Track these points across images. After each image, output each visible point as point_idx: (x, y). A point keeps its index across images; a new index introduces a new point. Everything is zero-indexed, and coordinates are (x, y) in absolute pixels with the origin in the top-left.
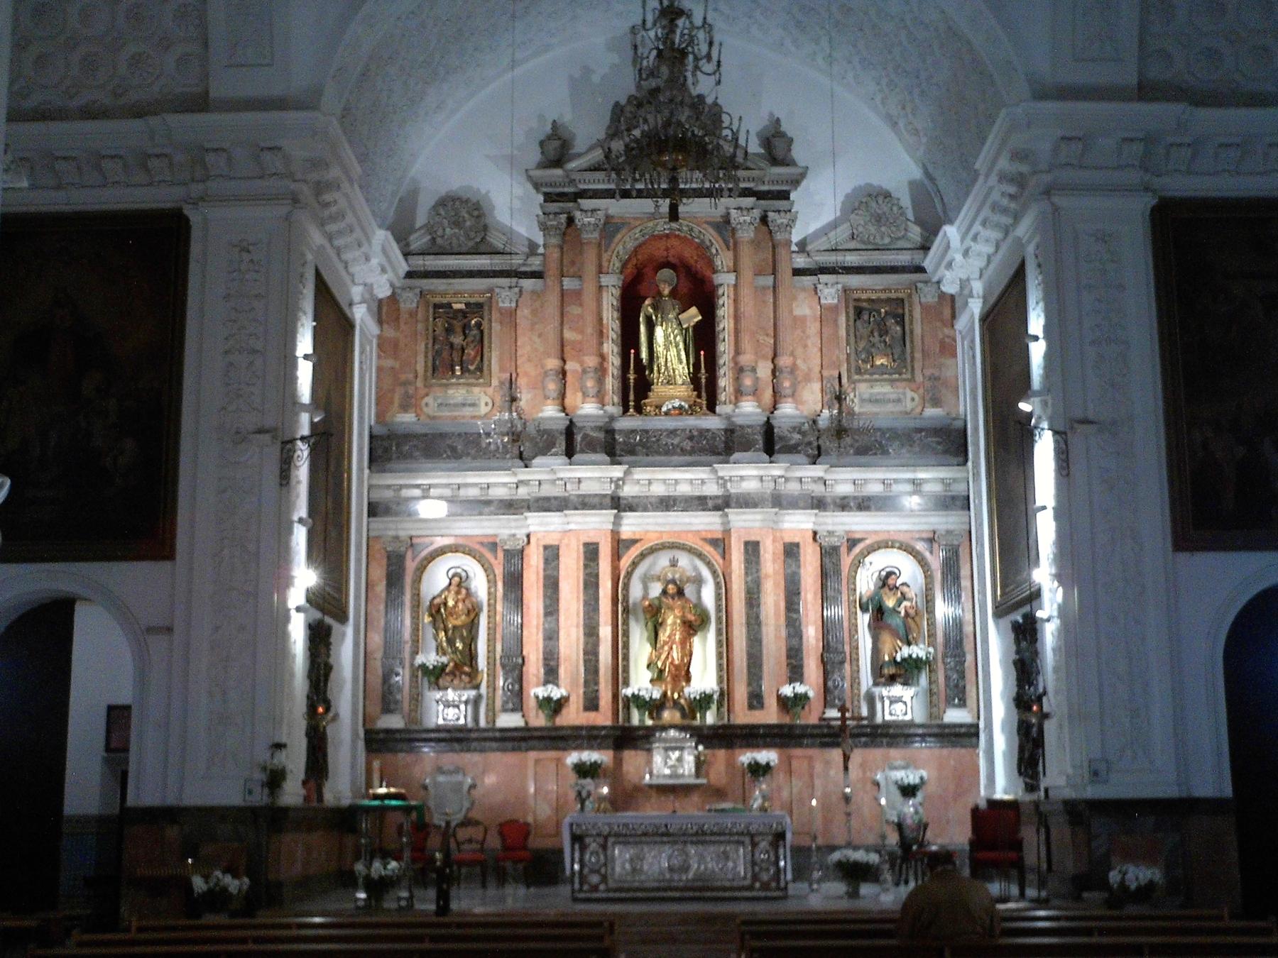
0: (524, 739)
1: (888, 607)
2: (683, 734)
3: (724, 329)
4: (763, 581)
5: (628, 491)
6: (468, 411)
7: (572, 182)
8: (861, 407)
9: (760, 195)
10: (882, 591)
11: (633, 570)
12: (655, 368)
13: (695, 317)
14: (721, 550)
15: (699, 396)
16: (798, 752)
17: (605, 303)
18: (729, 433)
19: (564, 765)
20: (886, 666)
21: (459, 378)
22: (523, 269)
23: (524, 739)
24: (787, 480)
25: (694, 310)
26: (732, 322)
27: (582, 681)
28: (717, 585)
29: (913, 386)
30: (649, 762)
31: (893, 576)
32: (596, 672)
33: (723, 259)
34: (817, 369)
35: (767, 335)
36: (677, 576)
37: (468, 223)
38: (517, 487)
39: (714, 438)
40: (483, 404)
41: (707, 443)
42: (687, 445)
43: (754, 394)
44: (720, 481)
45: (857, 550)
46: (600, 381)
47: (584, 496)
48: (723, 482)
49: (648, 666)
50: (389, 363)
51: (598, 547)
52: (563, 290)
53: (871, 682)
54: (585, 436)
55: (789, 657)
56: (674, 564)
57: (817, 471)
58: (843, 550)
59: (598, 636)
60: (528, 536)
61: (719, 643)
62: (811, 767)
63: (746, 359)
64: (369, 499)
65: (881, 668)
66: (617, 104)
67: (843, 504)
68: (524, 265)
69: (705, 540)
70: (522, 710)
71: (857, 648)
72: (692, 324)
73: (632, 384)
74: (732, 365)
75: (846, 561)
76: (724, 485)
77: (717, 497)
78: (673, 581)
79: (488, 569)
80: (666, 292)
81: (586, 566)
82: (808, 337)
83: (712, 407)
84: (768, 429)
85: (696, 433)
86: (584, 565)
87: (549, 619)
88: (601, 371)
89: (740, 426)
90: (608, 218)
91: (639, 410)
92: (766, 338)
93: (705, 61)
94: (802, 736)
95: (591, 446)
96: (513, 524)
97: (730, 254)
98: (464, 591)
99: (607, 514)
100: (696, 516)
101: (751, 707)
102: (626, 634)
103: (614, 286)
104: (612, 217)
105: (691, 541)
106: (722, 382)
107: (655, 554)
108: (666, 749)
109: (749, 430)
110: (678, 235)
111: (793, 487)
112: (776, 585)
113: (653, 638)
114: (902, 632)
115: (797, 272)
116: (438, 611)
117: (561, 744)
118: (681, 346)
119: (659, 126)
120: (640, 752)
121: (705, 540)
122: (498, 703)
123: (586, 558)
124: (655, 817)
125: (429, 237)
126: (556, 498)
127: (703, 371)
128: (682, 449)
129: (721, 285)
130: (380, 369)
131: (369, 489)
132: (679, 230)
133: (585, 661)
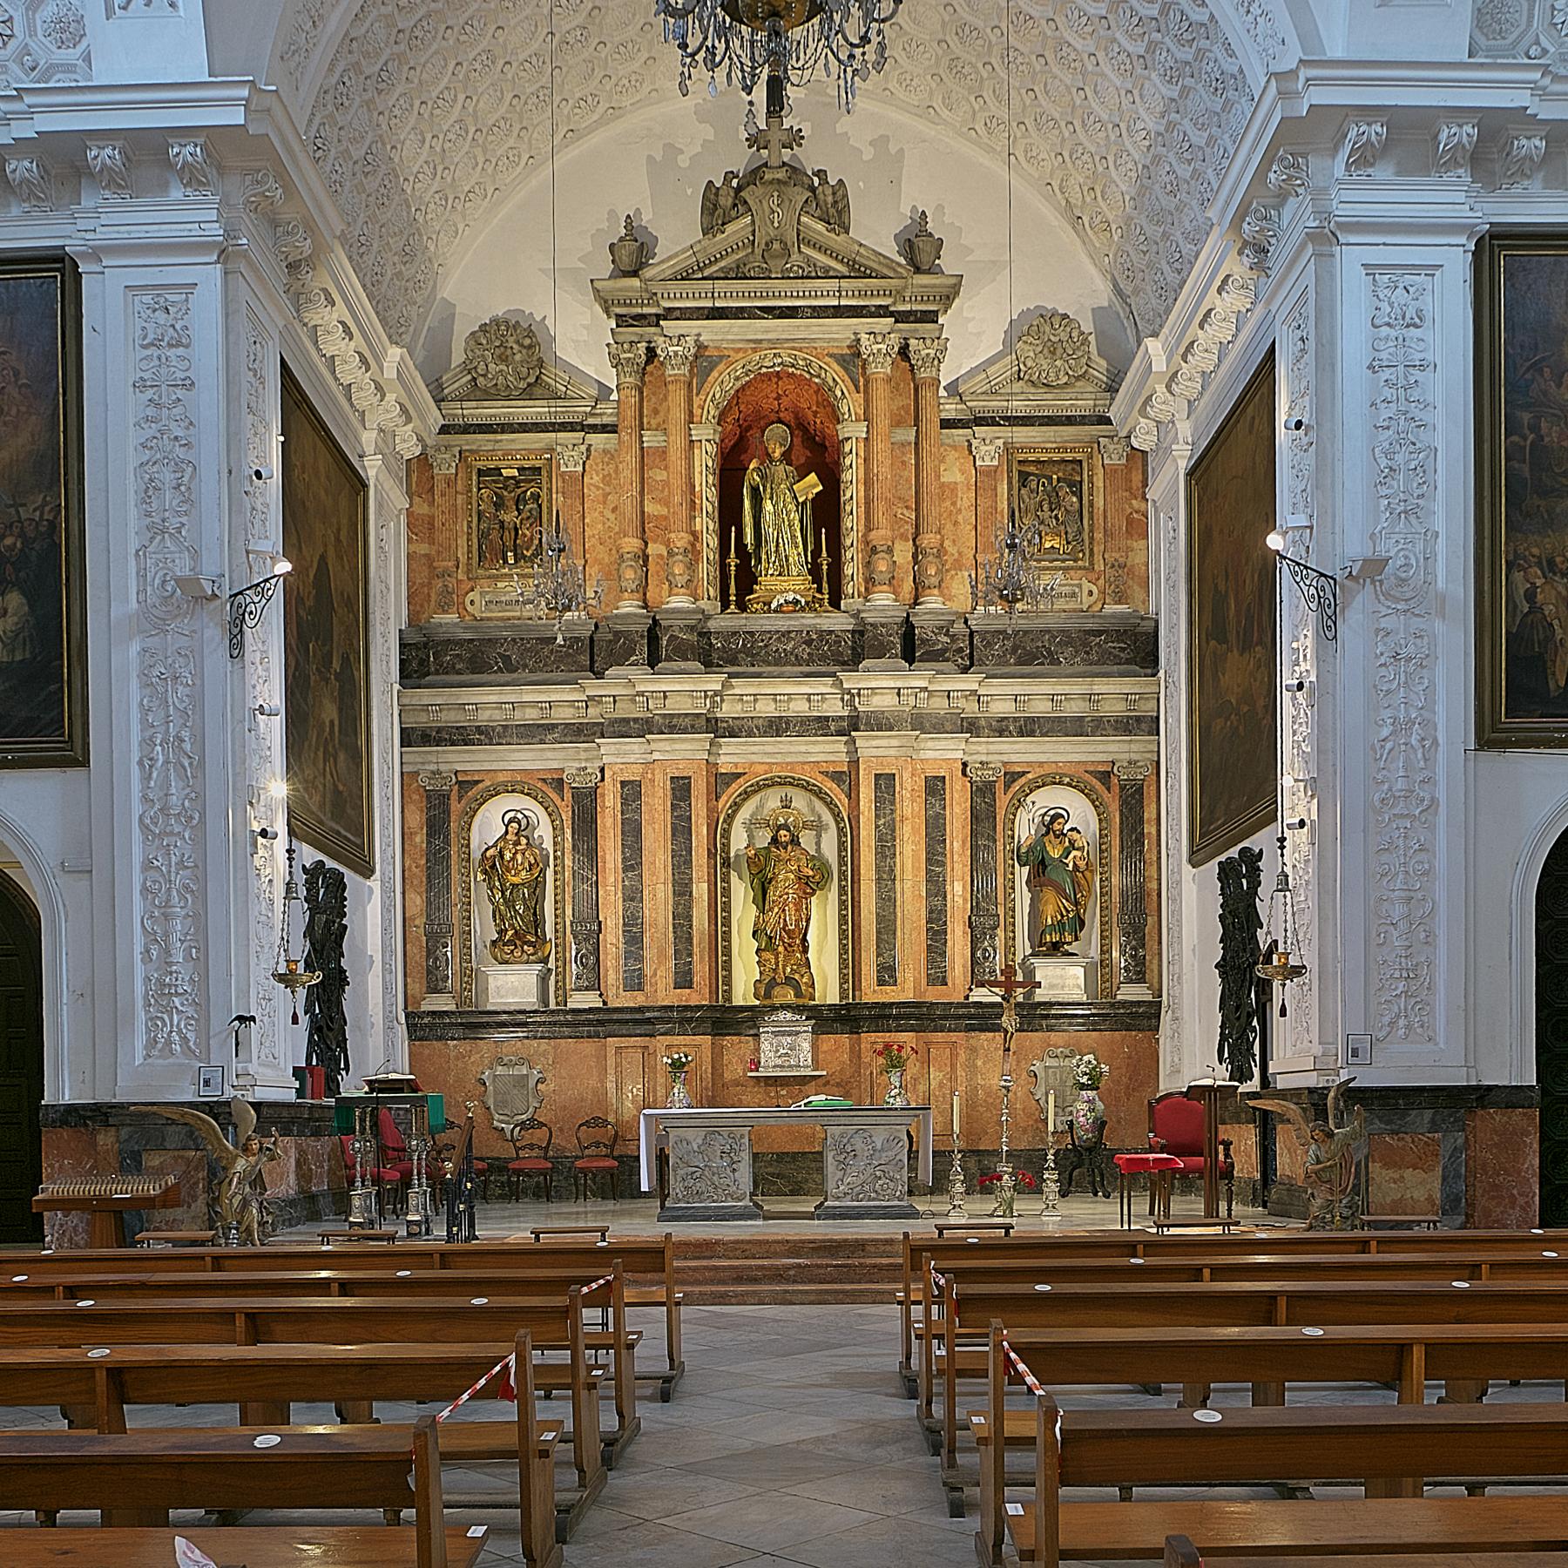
4: (898, 825)
5: (728, 710)
9: (901, 317)
10: (1046, 839)
11: (735, 812)
13: (815, 486)
14: (846, 788)
15: (819, 590)
17: (697, 464)
18: (857, 636)
20: (1047, 930)
22: (591, 421)
26: (862, 488)
28: (841, 831)
29: (1093, 576)
31: (1061, 820)
32: (690, 940)
35: (907, 507)
37: (518, 357)
45: (1016, 786)
46: (692, 566)
50: (423, 548)
57: (970, 682)
58: (1000, 786)
60: (602, 770)
61: (842, 903)
62: (954, 1056)
63: (879, 536)
67: (1001, 728)
69: (826, 774)
75: (1002, 801)
76: (851, 703)
78: (786, 827)
83: (835, 603)
84: (908, 628)
85: (814, 637)
91: (742, 607)
95: (682, 651)
96: (583, 755)
101: (881, 982)
102: (727, 892)
103: (708, 441)
106: (848, 570)
111: (939, 704)
115: (947, 424)
116: (493, 866)
117: (647, 1028)
121: (826, 774)
122: (571, 982)
123: (674, 796)
126: (636, 720)
127: (824, 554)
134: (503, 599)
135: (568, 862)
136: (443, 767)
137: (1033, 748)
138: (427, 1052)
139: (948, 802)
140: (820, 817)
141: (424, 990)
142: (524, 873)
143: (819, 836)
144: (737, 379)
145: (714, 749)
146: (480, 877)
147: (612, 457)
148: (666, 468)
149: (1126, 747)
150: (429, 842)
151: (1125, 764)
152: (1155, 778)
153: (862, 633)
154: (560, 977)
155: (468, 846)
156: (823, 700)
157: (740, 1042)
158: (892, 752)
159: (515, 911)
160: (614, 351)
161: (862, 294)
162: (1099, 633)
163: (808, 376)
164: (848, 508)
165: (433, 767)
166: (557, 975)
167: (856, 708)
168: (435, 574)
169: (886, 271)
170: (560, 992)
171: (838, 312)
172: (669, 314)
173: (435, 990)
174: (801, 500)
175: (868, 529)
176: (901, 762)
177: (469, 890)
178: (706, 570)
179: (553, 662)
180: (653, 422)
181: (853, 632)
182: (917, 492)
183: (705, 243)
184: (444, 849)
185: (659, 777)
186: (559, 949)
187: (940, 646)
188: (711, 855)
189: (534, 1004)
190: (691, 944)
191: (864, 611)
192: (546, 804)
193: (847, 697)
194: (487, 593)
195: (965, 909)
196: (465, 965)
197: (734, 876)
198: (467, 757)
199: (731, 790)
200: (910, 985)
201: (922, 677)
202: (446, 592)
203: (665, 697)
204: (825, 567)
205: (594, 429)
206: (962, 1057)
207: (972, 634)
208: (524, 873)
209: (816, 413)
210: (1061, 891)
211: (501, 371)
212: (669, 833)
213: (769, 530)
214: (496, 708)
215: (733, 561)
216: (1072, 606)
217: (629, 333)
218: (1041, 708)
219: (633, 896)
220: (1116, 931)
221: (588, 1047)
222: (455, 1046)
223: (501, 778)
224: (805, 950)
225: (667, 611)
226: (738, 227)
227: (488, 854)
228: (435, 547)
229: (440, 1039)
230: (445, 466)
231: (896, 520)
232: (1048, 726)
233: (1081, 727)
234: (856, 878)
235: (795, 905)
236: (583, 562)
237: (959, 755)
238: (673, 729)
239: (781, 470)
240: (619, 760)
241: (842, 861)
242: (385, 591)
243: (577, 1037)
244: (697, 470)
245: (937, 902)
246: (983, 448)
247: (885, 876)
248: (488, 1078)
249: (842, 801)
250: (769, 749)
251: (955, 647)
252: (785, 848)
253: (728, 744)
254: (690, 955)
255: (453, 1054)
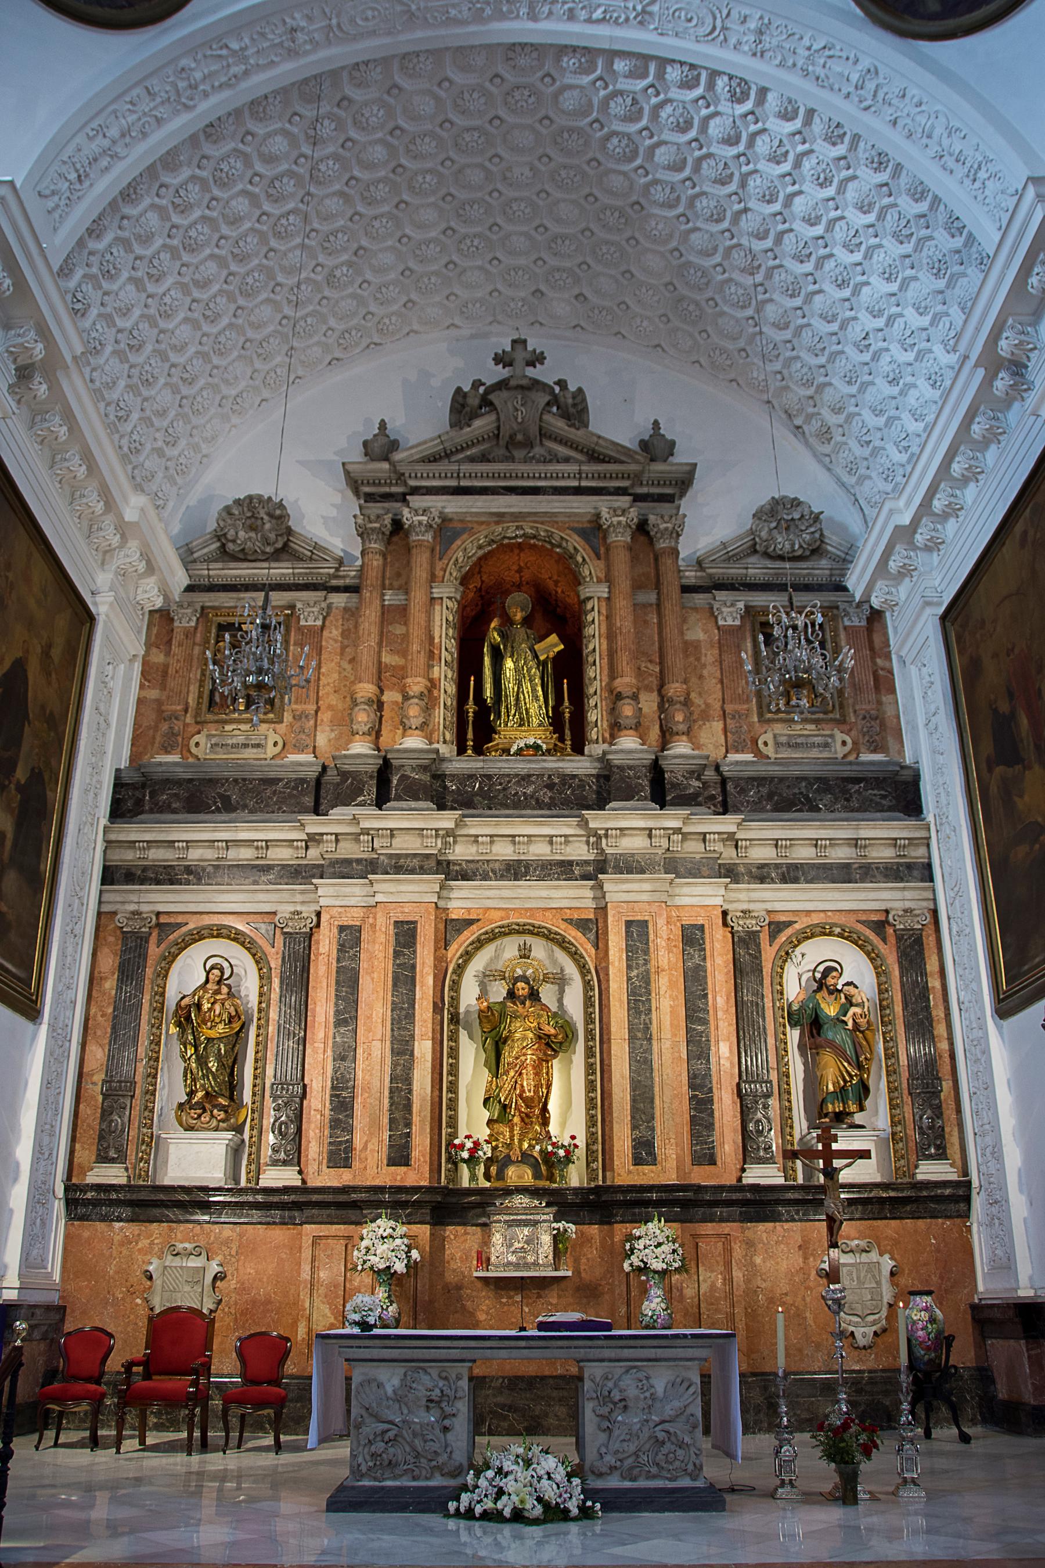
0: (297, 1206)
1: (828, 1016)
2: (537, 1202)
3: (594, 650)
4: (653, 977)
5: (461, 852)
6: (250, 753)
7: (400, 477)
8: (776, 752)
9: (638, 498)
10: (818, 996)
11: (466, 962)
12: (503, 710)
13: (556, 645)
14: (592, 937)
15: (562, 739)
16: (708, 1228)
17: (437, 618)
18: (602, 780)
19: (501, 617)
20: (829, 1098)
21: (241, 712)
22: (334, 582)
23: (297, 1206)
24: (685, 836)
25: (553, 638)
26: (605, 643)
27: (386, 1120)
28: (587, 985)
29: (846, 727)
30: (486, 1242)
31: (834, 974)
32: (408, 1107)
33: (591, 568)
34: (717, 705)
35: (651, 661)
36: (529, 972)
37: (267, 526)
38: (307, 848)
39: (582, 787)
40: (270, 743)
41: (572, 793)
42: (545, 795)
43: (636, 729)
44: (592, 839)
45: (783, 938)
46: (428, 710)
47: (398, 856)
48: (595, 838)
49: (486, 1101)
50: (153, 694)
51: (415, 928)
52: (380, 662)
53: (805, 1125)
54: (404, 778)
55: (692, 1086)
56: (525, 953)
57: (727, 824)
58: (764, 937)
59: (412, 1054)
60: (318, 914)
61: (590, 1068)
62: (728, 1251)
63: (625, 682)
64: (105, 860)
65: (823, 1101)
66: (459, 390)
67: (762, 874)
68: (336, 577)
69: (569, 921)
70: (299, 1164)
71: (788, 1076)
72: (552, 654)
73: (471, 719)
74: (605, 694)
75: (769, 953)
76: (597, 845)
77: (587, 862)
78: (524, 979)
79: (260, 961)
80: (519, 616)
81: (397, 954)
82: (704, 666)
83: (578, 749)
84: (656, 770)
85: (557, 781)
86: (395, 951)
87: (342, 1030)
88: (429, 699)
89: (618, 767)
90: (445, 519)
91: (479, 751)
92: (649, 665)
93: (398, 456)
94: (581, 1206)
95: (412, 792)
96: (299, 898)
97: (601, 564)
98: (225, 990)
99: (429, 881)
100: (556, 887)
101: (638, 1161)
102: (454, 1053)
103: (450, 598)
104: (451, 520)
105: (550, 923)
106: (592, 716)
107: (498, 942)
108: (510, 1224)
109: (631, 773)
110: (534, 545)
111: (694, 848)
112: (672, 985)
113: (494, 1062)
114: (850, 1051)
115: (686, 589)
116: (188, 1018)
117: (353, 1214)
118: (537, 681)
119: (68, 1561)
120: (470, 1229)
121: (569, 921)
122: (267, 1153)
123: (398, 943)
124: (483, 426)
125: (218, 544)
126: (359, 861)
127: (566, 703)
128: (537, 800)
129: (589, 598)
130: (140, 701)
131: (234, 558)
132: (534, 537)
133: (391, 1091)
134: (230, 742)
135: (273, 1015)
136: (145, 908)
137: (798, 895)
138: (86, 1234)
139: (708, 953)
140: (562, 970)
141: (93, 1158)
142: (221, 1026)
143: (562, 992)
144: (480, 547)
145: (444, 893)
146: (173, 1030)
147: (353, 615)
148: (406, 624)
149: (898, 895)
150: (119, 989)
151: (901, 913)
152: (932, 927)
153: (607, 778)
154: (254, 1149)
155: (163, 994)
156: (567, 842)
157: (466, 1233)
158: (645, 897)
159: (208, 1069)
160: (360, 521)
161: (601, 477)
162: (857, 780)
163: (548, 546)
164: (591, 659)
165: (132, 907)
166: (251, 1146)
167: (603, 850)
168: (162, 715)
169: (623, 458)
170: (253, 1167)
171: (578, 491)
172: (415, 491)
173: (103, 1158)
174: (542, 658)
175: (613, 676)
176: (654, 908)
177: (158, 1044)
178: (442, 716)
179: (275, 803)
180: (396, 584)
181: (598, 777)
182: (661, 648)
183: (453, 434)
184: (136, 996)
185: (381, 920)
186: (256, 1115)
187: (692, 791)
188: (438, 1008)
189: (220, 1180)
190: (410, 1112)
191: (609, 753)
192: (253, 951)
193: (592, 839)
194: (214, 736)
195: (732, 1075)
196: (145, 1130)
197: (463, 1035)
198: (171, 897)
199: (462, 937)
200: (672, 1164)
201: (675, 817)
202: (172, 734)
203: (392, 836)
204: (567, 715)
205: (337, 589)
206: (738, 1251)
207: (724, 781)
208: (221, 1026)
209: (556, 583)
210: (839, 1052)
211: (250, 538)
212: (390, 979)
213: (509, 685)
214: (209, 847)
215: (471, 708)
216: (826, 755)
217: (375, 509)
218: (804, 854)
219: (345, 1054)
220: (908, 1099)
221: (279, 1234)
222: (121, 1229)
223: (207, 920)
224: (545, 1122)
225: (398, 751)
226: (482, 424)
227: (183, 1003)
228: (166, 693)
229: (104, 1219)
230: (186, 620)
231: (639, 673)
232: (813, 873)
233: (849, 874)
234: (605, 1037)
235: (534, 1068)
236: (315, 707)
237: (719, 901)
238: (398, 869)
239: (520, 632)
240: (338, 903)
241: (589, 1019)
242: (103, 725)
243: (268, 1223)
244: (437, 623)
245: (699, 1066)
246: (724, 609)
247: (639, 1035)
248: (156, 1269)
249: (588, 951)
250: (506, 893)
251: (706, 794)
252: (523, 1003)
253: (460, 888)
254: (408, 1125)
255: (117, 1238)
